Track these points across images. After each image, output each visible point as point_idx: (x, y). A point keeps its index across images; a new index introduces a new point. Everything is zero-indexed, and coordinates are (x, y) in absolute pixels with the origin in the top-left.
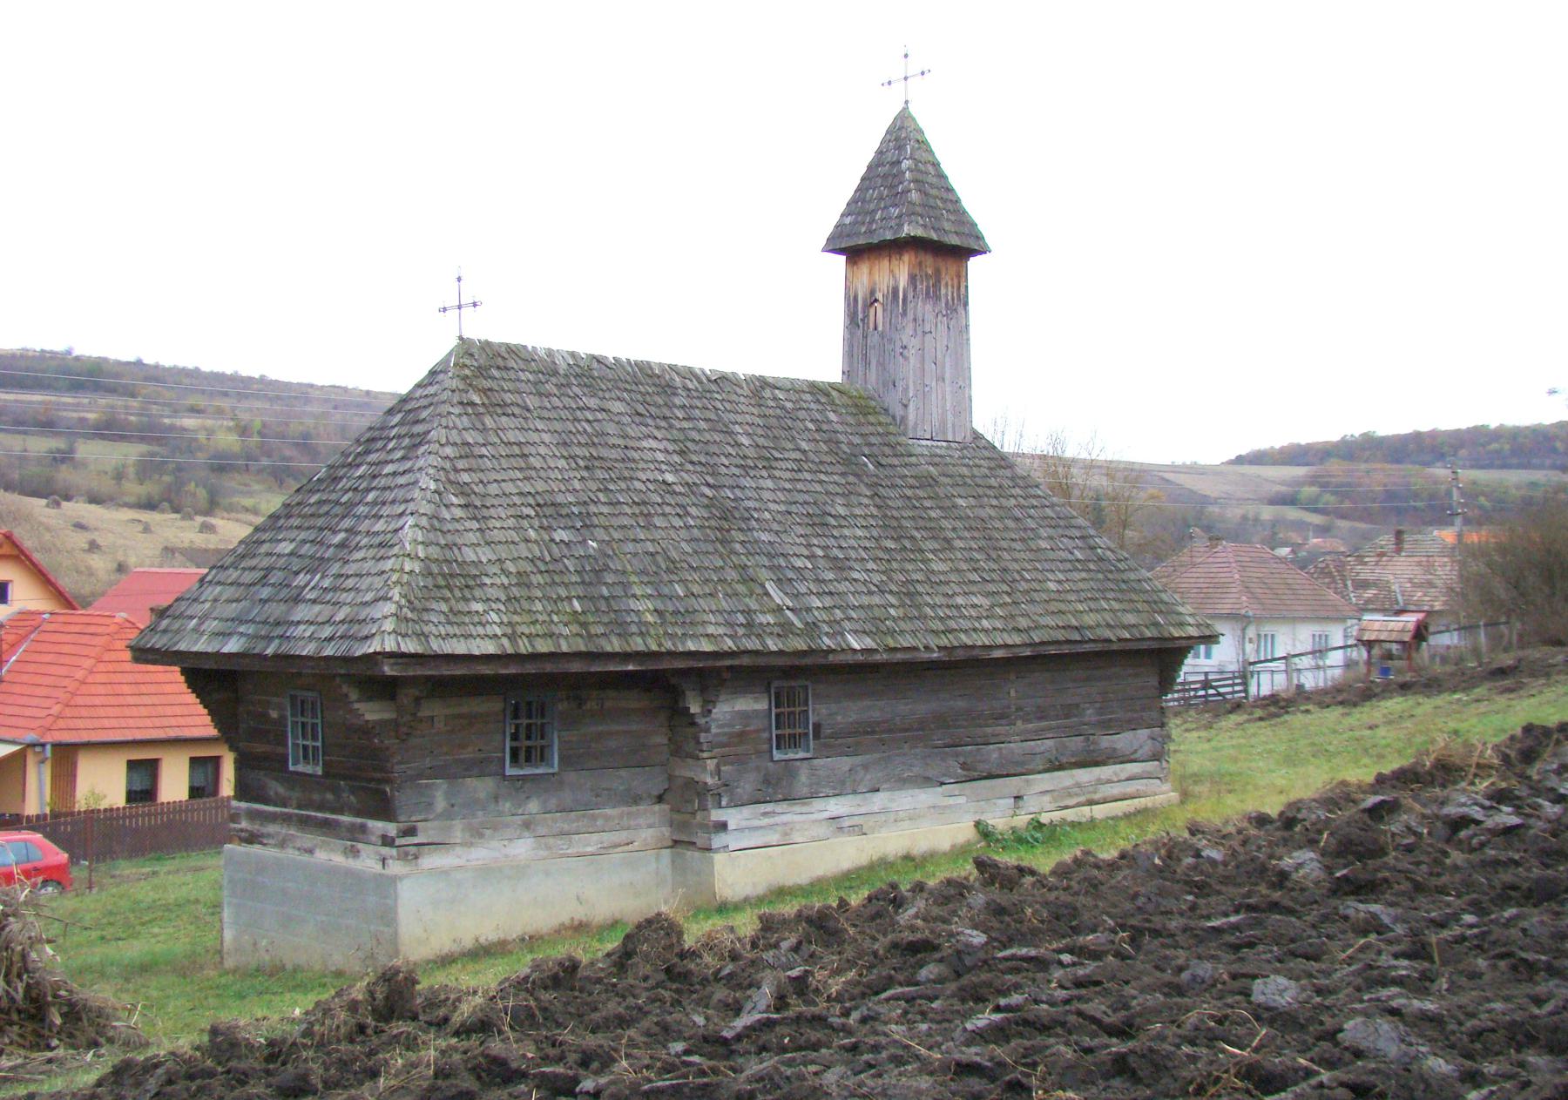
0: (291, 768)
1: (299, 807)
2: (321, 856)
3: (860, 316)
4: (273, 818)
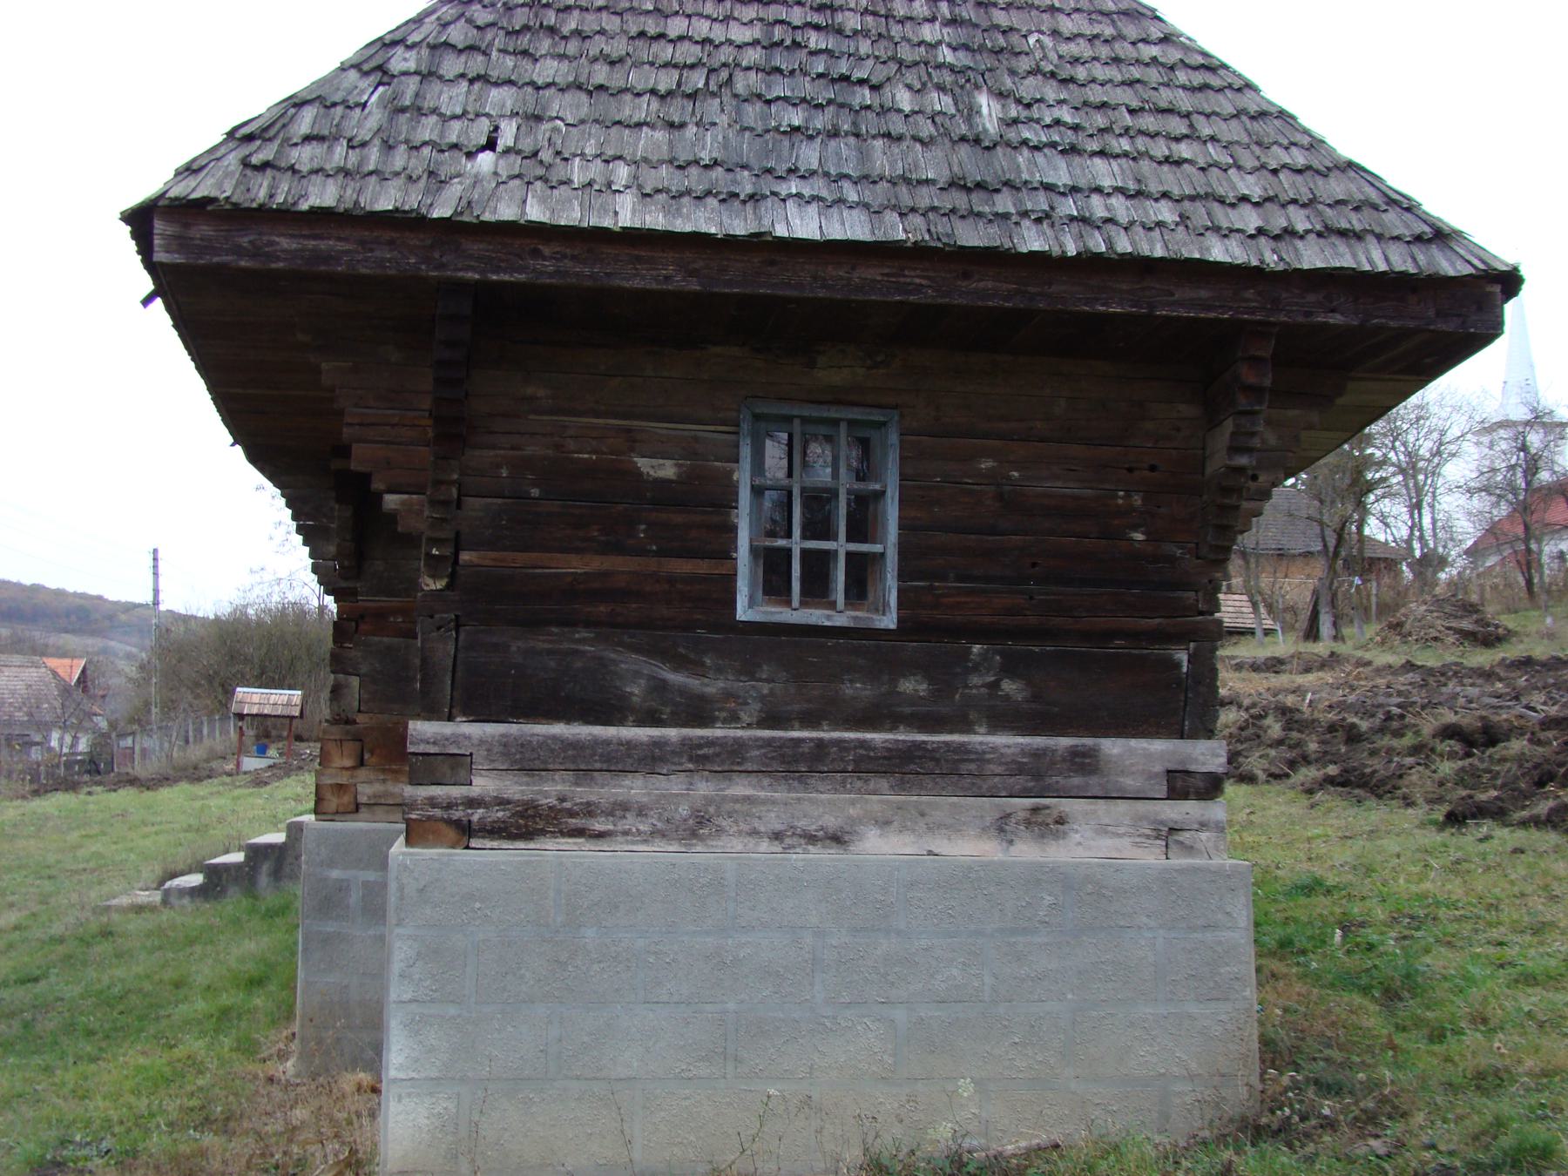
2: (879, 846)
4: (651, 760)
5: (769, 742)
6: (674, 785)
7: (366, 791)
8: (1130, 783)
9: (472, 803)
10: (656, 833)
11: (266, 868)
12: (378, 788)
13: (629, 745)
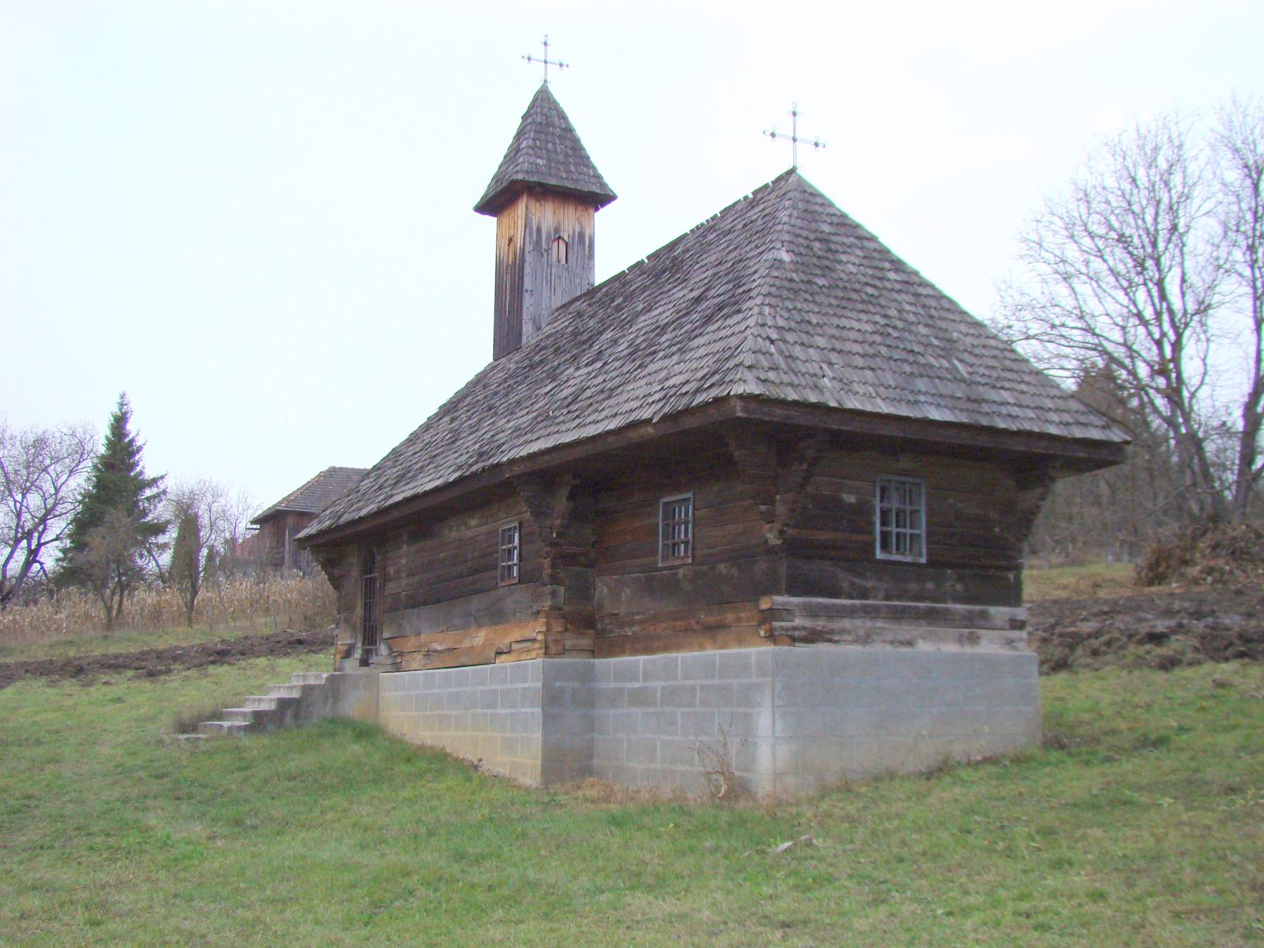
0: (879, 555)
2: (924, 647)
3: (544, 247)
4: (850, 612)
5: (887, 606)
6: (858, 622)
7: (568, 643)
8: (999, 623)
9: (795, 629)
10: (855, 641)
11: (290, 713)
12: (574, 641)
13: (844, 606)
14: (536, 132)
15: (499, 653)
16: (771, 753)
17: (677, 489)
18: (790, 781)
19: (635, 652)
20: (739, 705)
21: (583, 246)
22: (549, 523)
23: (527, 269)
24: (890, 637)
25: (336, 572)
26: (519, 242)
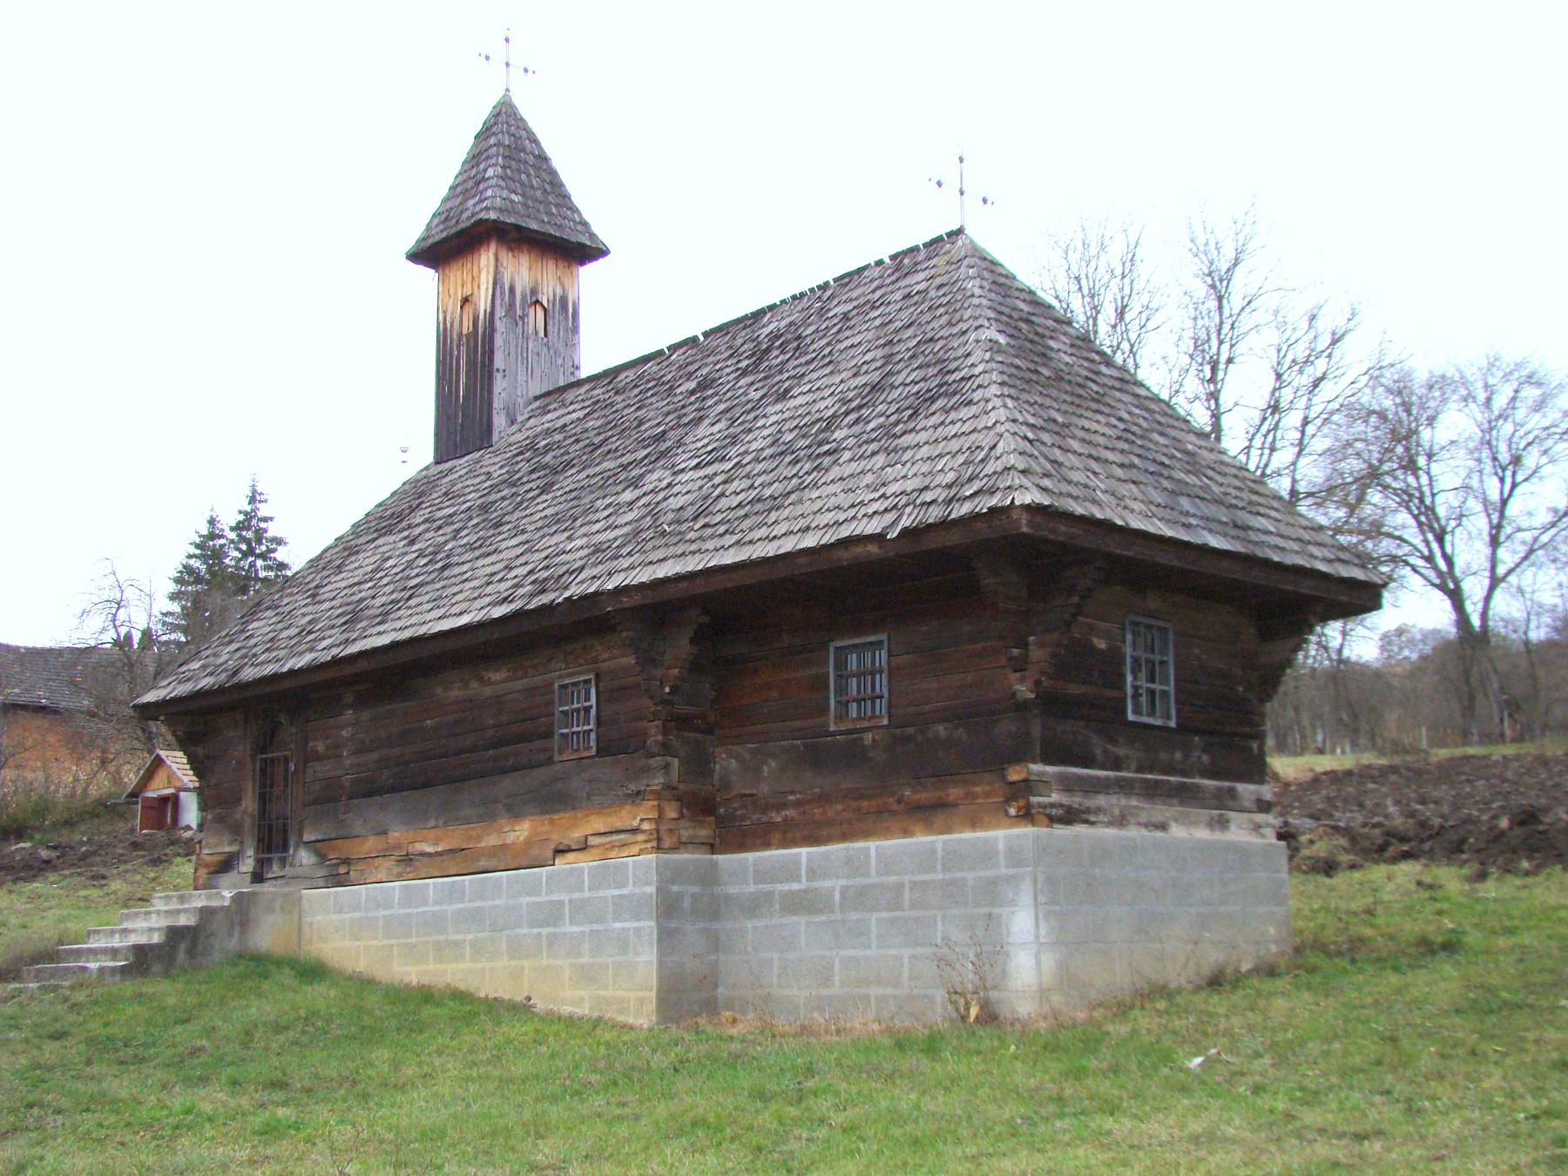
0: (1131, 717)
1: (1138, 771)
2: (1177, 831)
3: (519, 312)
6: (1113, 799)
8: (1247, 804)
9: (1052, 805)
11: (183, 946)
12: (691, 832)
13: (1098, 778)
14: (504, 157)
15: (560, 851)
16: (1028, 960)
17: (858, 628)
18: (1056, 999)
19: (786, 843)
20: (991, 905)
21: (564, 315)
22: (658, 673)
23: (499, 341)
24: (1144, 818)
25: (200, 751)
26: (483, 303)
